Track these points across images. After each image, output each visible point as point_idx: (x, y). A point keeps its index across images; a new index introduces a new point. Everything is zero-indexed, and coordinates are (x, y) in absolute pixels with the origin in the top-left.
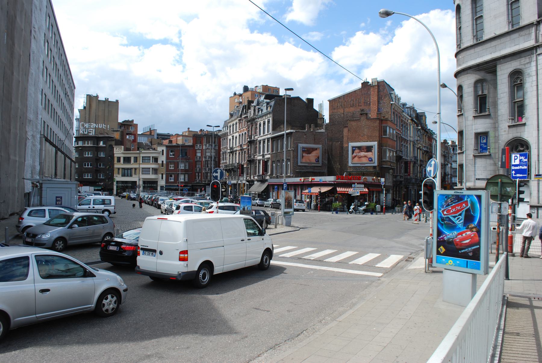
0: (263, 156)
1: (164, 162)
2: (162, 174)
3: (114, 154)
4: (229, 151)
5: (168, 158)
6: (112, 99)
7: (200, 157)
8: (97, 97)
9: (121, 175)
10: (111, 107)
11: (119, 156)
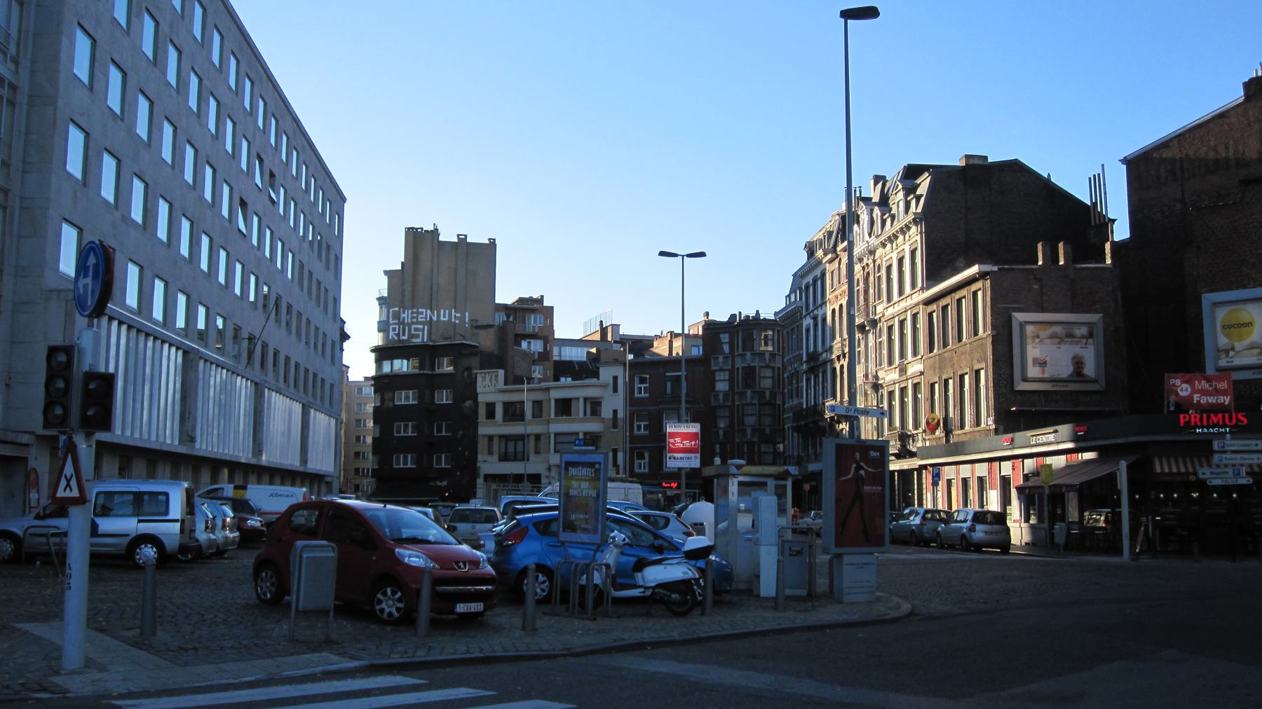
0: (903, 370)
1: (620, 415)
2: (615, 451)
3: (476, 395)
4: (805, 367)
5: (632, 401)
6: (477, 236)
7: (726, 395)
8: (435, 233)
9: (495, 457)
10: (477, 259)
11: (490, 399)
